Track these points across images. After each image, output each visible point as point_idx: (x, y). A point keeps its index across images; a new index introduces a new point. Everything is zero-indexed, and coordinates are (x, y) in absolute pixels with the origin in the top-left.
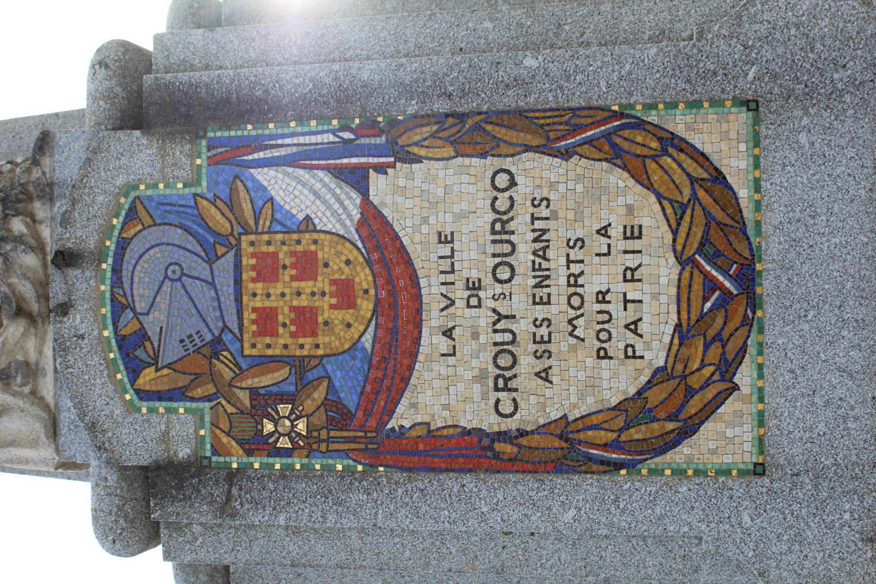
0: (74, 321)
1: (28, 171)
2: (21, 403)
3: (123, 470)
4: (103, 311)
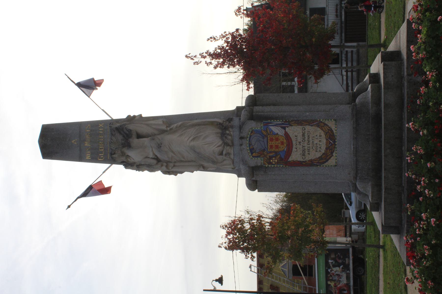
3: (249, 167)
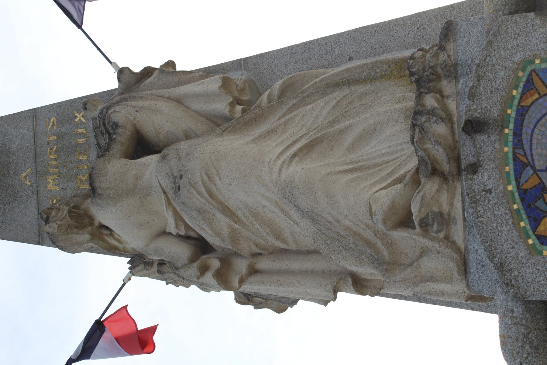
0: (482, 178)
1: (436, 55)
2: (437, 246)
3: (527, 303)
4: (507, 169)
